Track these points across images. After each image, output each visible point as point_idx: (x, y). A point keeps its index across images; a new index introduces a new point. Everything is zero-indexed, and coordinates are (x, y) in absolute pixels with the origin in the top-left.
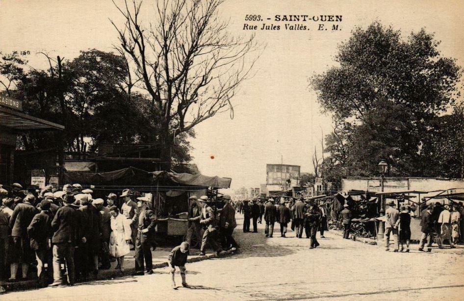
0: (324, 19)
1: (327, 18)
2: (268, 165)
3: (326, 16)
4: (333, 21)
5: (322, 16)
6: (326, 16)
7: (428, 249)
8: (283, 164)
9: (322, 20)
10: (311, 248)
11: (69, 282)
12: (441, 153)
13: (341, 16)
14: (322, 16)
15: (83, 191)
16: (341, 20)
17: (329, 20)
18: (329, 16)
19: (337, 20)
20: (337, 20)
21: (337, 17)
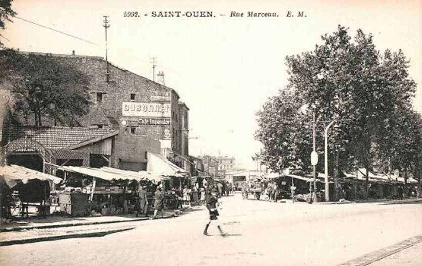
0: (196, 14)
1: (200, 14)
3: (198, 12)
4: (205, 16)
6: (198, 12)
9: (194, 15)
13: (212, 12)
14: (194, 12)
16: (211, 15)
17: (201, 16)
18: (201, 12)
19: (208, 16)
20: (169, 16)
21: (170, 13)
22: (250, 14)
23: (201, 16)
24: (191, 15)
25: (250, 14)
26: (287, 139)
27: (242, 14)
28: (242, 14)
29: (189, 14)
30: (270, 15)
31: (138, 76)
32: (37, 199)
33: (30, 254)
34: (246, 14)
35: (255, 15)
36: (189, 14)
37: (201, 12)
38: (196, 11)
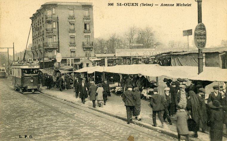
0: (129, 5)
1: (131, 4)
2: (184, 31)
3: (130, 3)
4: (134, 5)
5: (128, 3)
6: (130, 3)
7: (136, 117)
8: (127, 116)
9: (128, 5)
10: (83, 45)
11: (161, 64)
12: (211, 73)
13: (138, 4)
14: (128, 3)
15: (99, 135)
16: (137, 5)
17: (132, 5)
18: (132, 4)
19: (136, 5)
20: (136, 5)
21: (136, 4)
22: (178, 5)
23: (132, 5)
24: (127, 5)
25: (178, 5)
26: (206, 122)
27: (173, 5)
28: (173, 5)
29: (125, 5)
30: (168, 5)
31: (198, 13)
32: (89, 49)
33: (180, 27)
34: (175, 5)
35: (181, 5)
36: (125, 5)
37: (132, 4)
38: (129, 3)
